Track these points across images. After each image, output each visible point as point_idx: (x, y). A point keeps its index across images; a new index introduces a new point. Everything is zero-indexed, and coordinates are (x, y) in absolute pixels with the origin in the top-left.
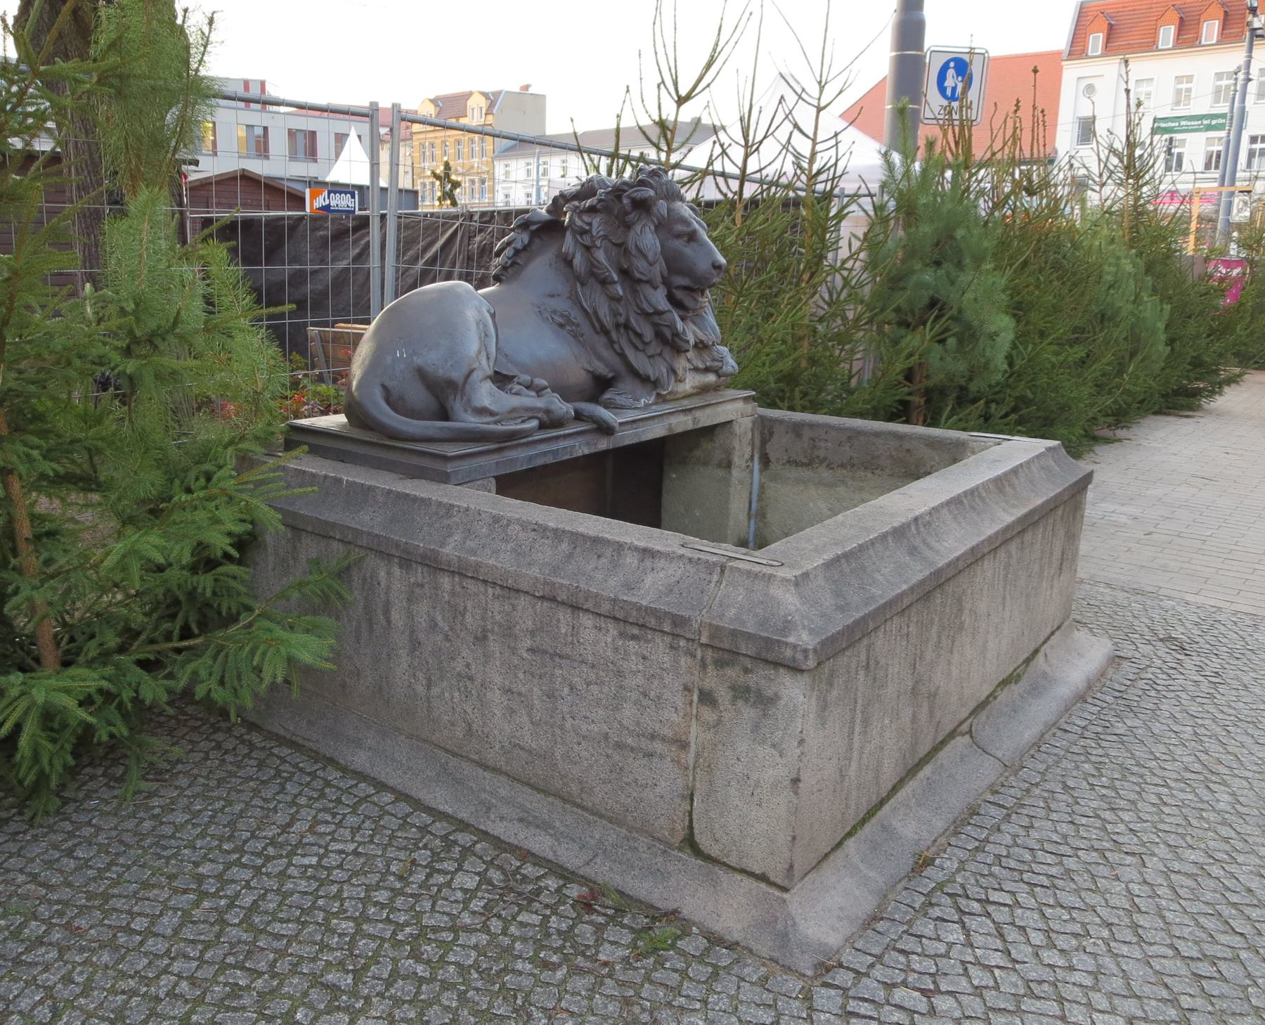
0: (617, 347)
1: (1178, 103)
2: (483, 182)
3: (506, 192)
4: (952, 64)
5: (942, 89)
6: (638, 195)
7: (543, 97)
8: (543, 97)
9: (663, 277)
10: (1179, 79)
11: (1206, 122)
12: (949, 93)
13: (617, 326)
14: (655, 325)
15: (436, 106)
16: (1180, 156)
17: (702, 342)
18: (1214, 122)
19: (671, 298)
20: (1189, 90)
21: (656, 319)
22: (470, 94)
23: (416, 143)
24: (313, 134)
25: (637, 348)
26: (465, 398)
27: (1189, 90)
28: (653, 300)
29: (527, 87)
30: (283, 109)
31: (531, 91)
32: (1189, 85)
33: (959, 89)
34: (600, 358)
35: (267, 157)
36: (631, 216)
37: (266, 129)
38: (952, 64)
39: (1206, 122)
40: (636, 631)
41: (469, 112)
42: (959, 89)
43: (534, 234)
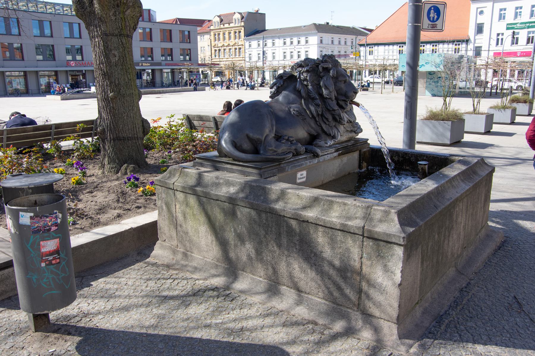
1: (516, 17)
2: (240, 49)
3: (250, 53)
4: (432, 8)
5: (429, 18)
7: (263, 15)
8: (263, 15)
9: (335, 96)
10: (517, 8)
11: (527, 25)
12: (431, 19)
13: (318, 115)
16: (517, 39)
17: (349, 120)
18: (531, 25)
19: (338, 104)
20: (520, 12)
24: (170, 31)
25: (326, 123)
27: (520, 12)
28: (332, 106)
32: (520, 10)
33: (435, 18)
34: (312, 128)
37: (151, 29)
38: (432, 8)
39: (527, 25)
40: (468, 193)
42: (435, 18)
43: (284, 81)
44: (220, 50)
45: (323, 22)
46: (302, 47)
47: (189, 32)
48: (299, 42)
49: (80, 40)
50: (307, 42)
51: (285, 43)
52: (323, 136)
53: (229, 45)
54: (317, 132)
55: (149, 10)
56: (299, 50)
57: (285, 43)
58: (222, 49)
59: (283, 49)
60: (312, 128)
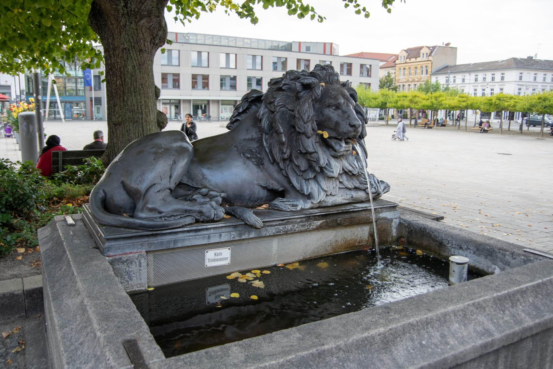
0: (284, 172)
6: (306, 81)
14: (309, 161)
15: (407, 52)
21: (308, 156)
22: (421, 48)
23: (397, 68)
26: (144, 201)
29: (448, 44)
30: (481, 69)
31: (450, 46)
34: (275, 179)
35: (370, 76)
36: (301, 94)
41: (421, 55)
44: (404, 86)
45: (524, 56)
46: (497, 84)
47: (370, 66)
48: (493, 79)
49: (261, 72)
50: (502, 78)
51: (476, 80)
52: (292, 193)
53: (414, 81)
54: (282, 186)
55: (331, 44)
56: (492, 87)
57: (476, 80)
58: (406, 84)
59: (482, 86)
60: (275, 179)
